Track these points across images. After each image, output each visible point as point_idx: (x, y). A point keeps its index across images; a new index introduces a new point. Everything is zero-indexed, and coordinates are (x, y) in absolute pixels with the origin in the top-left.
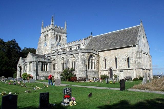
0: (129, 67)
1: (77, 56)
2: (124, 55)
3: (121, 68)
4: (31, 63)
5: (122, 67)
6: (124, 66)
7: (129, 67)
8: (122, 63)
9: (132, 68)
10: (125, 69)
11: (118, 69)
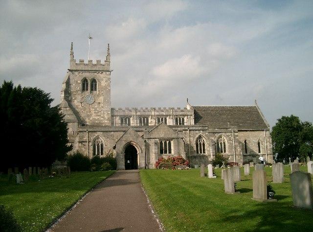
0: (259, 152)
7: (259, 152)
11: (248, 154)
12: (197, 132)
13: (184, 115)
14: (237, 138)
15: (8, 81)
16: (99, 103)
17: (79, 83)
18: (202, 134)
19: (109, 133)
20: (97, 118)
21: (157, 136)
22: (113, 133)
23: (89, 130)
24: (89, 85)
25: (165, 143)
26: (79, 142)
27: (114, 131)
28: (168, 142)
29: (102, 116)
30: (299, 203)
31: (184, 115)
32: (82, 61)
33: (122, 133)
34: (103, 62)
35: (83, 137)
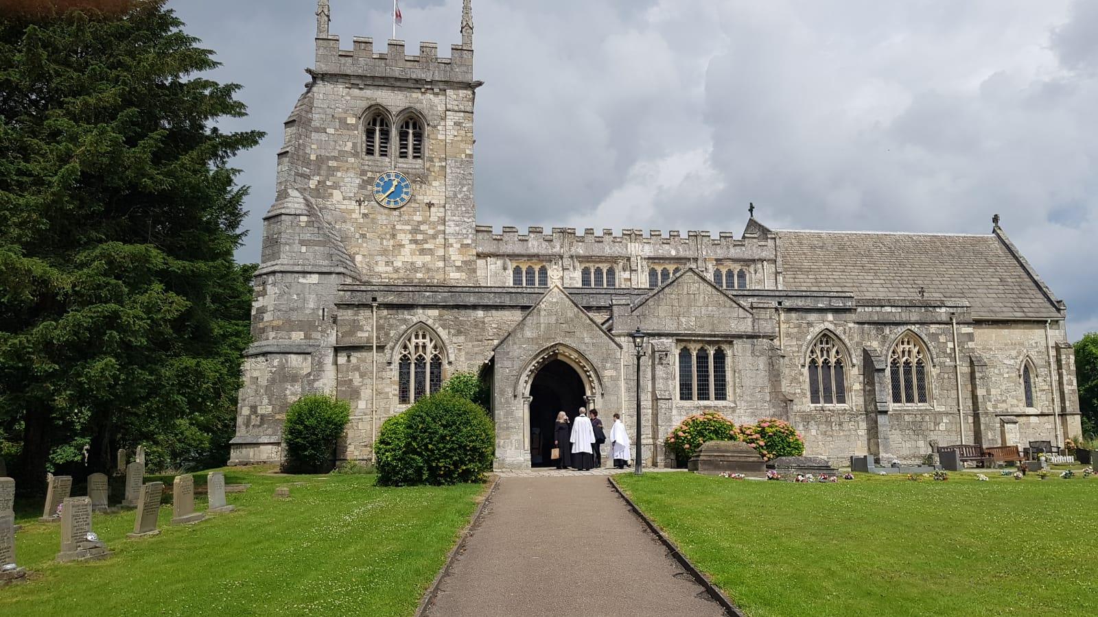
0: (1029, 403)
1: (934, 337)
2: (1014, 353)
3: (1002, 407)
4: (731, 343)
5: (1004, 401)
6: (1015, 402)
7: (1029, 403)
8: (1004, 387)
9: (1046, 411)
10: (1018, 410)
12: (812, 317)
13: (550, 258)
14: (971, 345)
15: (428, 39)
16: (430, 205)
17: (355, 127)
18: (831, 327)
19: (463, 315)
20: (419, 260)
21: (671, 327)
22: (480, 313)
23: (380, 300)
24: (395, 132)
25: (702, 358)
26: (337, 350)
27: (487, 307)
28: (711, 352)
29: (441, 252)
30: (70, 483)
31: (550, 258)
32: (397, 46)
33: (517, 315)
34: (444, 53)
35: (356, 327)
